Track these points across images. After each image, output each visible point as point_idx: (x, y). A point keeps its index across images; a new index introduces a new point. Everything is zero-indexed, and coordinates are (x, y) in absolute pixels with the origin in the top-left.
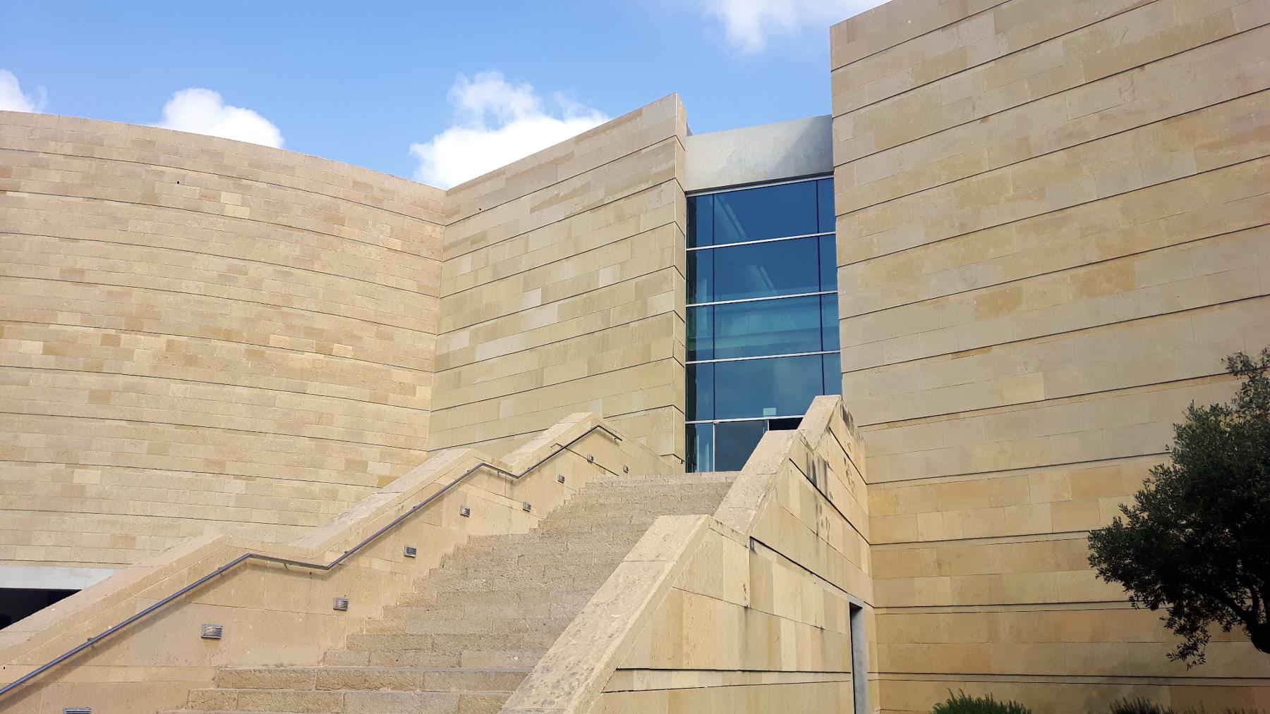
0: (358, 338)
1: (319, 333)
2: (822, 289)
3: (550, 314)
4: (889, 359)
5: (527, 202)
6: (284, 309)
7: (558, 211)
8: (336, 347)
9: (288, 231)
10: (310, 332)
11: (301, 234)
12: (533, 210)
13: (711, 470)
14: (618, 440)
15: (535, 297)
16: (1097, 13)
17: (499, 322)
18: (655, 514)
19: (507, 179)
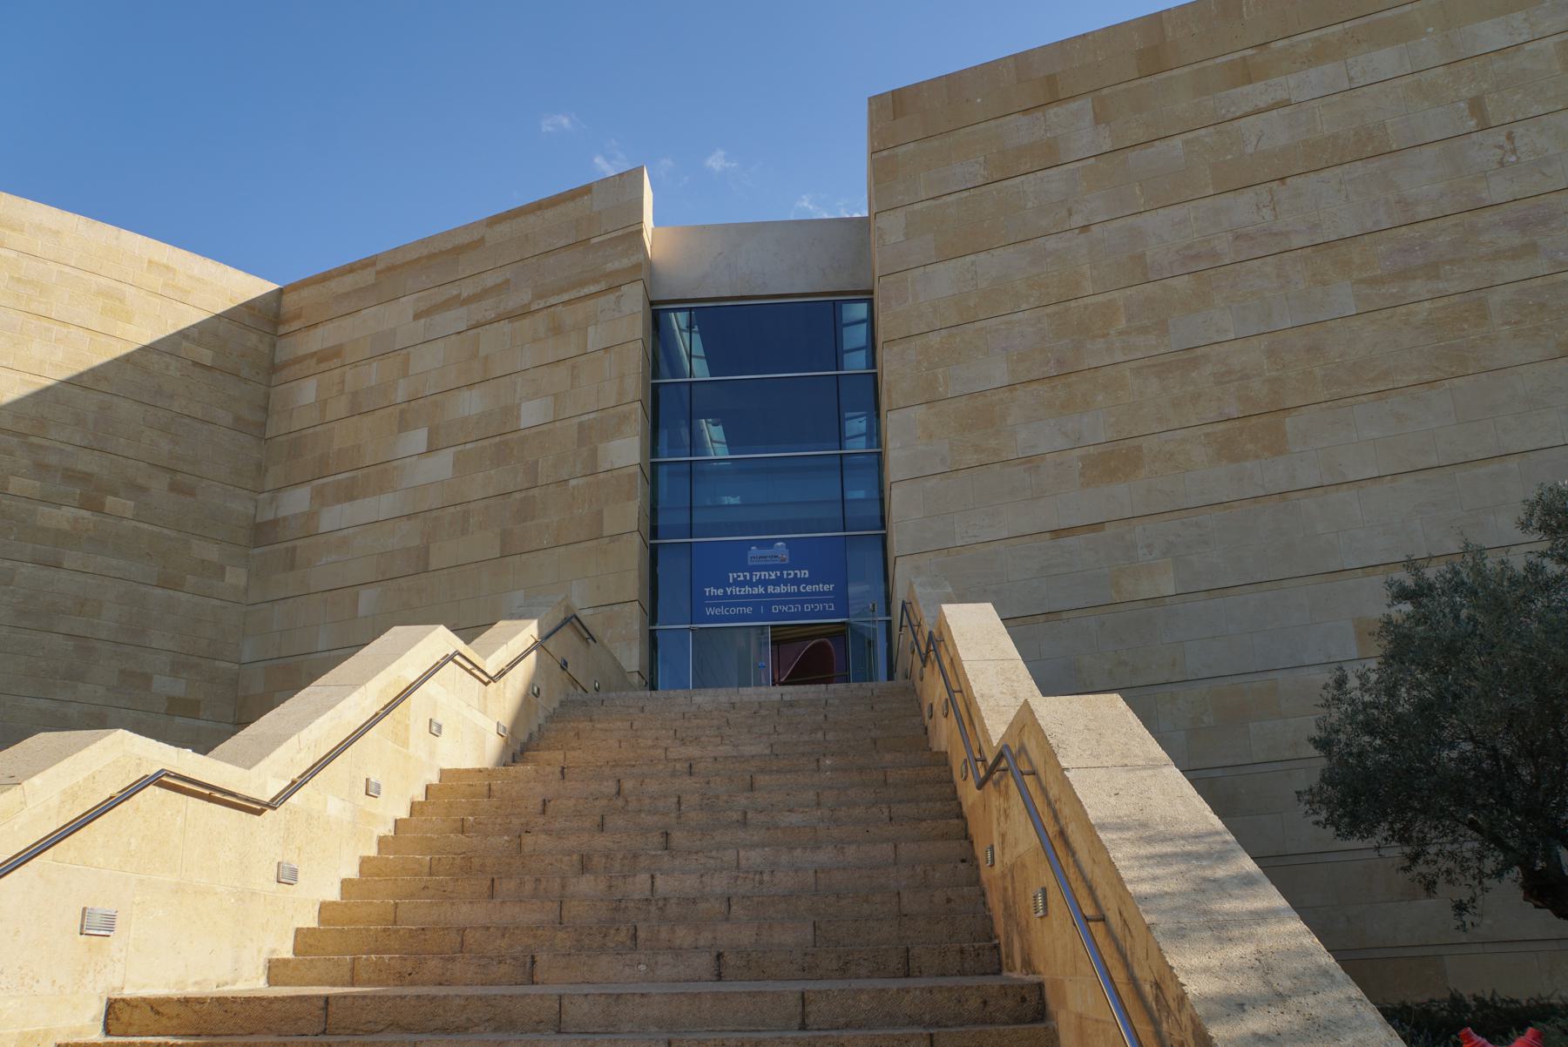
0: (143, 490)
1: (86, 478)
2: (693, 454)
3: (442, 465)
4: (962, 538)
5: (408, 304)
6: (33, 440)
7: (455, 319)
8: (110, 501)
9: (45, 323)
10: (71, 476)
11: (65, 330)
12: (417, 317)
13: (768, 684)
14: (590, 640)
15: (418, 439)
16: (1223, 111)
17: (360, 475)
18: (494, 770)
19: (378, 273)
